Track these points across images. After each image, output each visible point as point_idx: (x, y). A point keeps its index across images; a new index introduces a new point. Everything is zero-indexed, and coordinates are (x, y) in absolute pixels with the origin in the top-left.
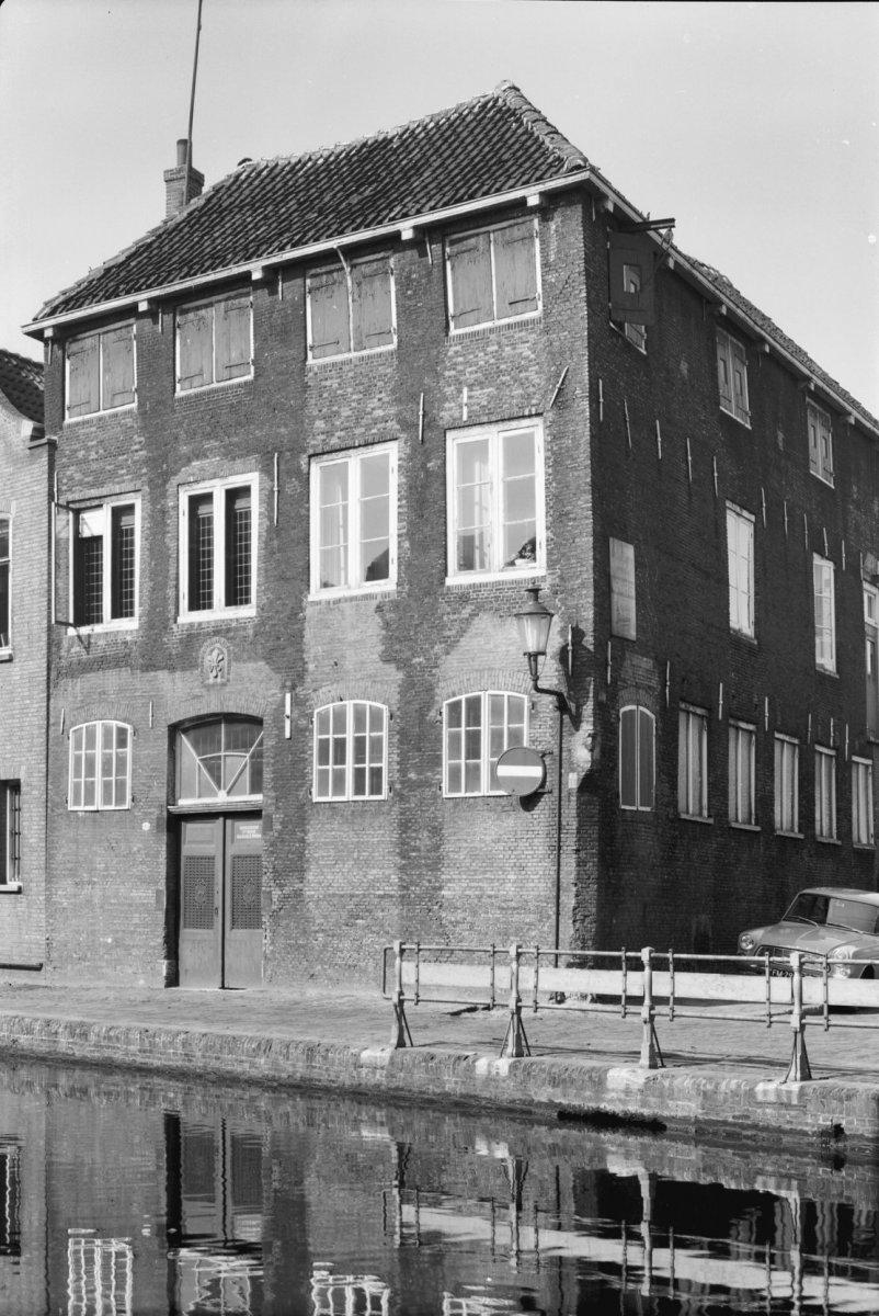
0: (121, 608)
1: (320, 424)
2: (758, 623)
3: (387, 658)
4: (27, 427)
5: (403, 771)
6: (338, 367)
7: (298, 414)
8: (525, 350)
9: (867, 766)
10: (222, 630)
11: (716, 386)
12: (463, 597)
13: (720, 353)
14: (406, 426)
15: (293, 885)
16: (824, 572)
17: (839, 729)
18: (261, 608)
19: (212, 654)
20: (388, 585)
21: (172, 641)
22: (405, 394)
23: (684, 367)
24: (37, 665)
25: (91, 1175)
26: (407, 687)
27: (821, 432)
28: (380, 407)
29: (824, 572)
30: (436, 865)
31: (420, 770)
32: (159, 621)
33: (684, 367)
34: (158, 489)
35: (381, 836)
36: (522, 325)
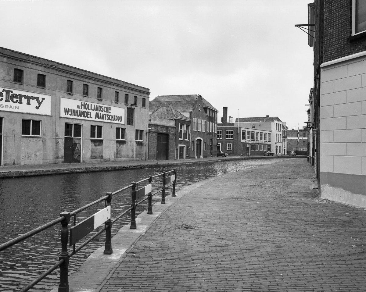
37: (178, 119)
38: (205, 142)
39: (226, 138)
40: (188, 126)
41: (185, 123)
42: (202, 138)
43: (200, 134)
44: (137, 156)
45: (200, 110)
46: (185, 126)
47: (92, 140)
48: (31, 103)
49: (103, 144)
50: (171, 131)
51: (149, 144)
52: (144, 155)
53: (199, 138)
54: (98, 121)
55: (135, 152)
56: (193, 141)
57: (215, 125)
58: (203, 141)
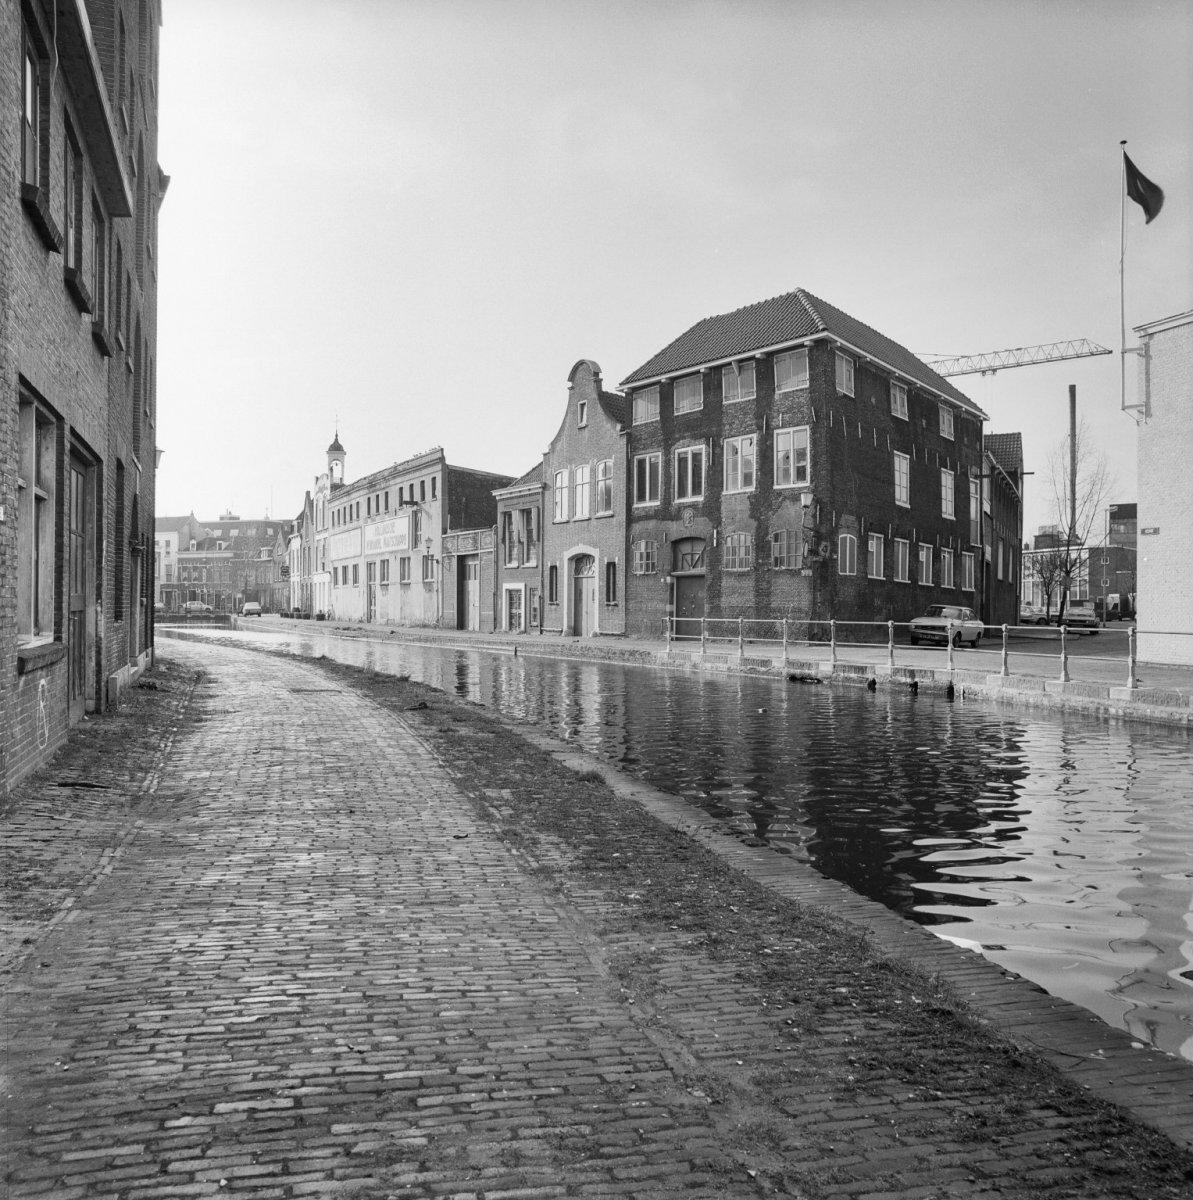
0: (653, 496)
1: (727, 427)
2: (912, 500)
3: (751, 517)
4: (619, 427)
5: (757, 559)
6: (734, 404)
7: (720, 425)
8: (802, 400)
9: (970, 557)
10: (693, 506)
11: (889, 404)
12: (780, 493)
13: (892, 391)
14: (760, 428)
15: (716, 602)
16: (947, 480)
17: (954, 540)
18: (706, 497)
19: (687, 514)
20: (752, 489)
21: (673, 509)
22: (759, 416)
23: (873, 400)
24: (622, 517)
25: (811, 839)
26: (758, 528)
27: (946, 416)
28: (750, 420)
29: (947, 480)
30: (768, 595)
31: (763, 559)
32: (667, 501)
33: (873, 400)
34: (667, 453)
35: (749, 584)
36: (801, 390)
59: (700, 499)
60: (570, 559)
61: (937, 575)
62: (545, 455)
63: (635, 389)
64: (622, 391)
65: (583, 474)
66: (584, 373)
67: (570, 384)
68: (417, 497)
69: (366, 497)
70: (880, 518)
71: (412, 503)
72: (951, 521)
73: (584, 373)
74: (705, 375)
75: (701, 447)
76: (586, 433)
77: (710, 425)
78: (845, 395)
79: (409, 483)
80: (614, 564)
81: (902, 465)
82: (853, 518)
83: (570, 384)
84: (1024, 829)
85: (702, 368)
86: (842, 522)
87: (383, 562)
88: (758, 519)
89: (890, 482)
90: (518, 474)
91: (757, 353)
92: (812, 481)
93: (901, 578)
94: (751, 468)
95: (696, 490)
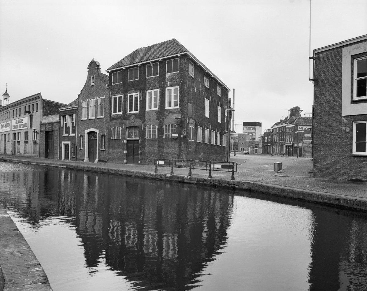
14: (160, 87)
16: (219, 108)
17: (221, 130)
19: (133, 118)
21: (127, 116)
22: (160, 82)
26: (159, 123)
29: (219, 108)
30: (163, 147)
37: (63, 110)
38: (103, 135)
39: (355, 152)
40: (71, 116)
41: (67, 114)
42: (97, 129)
43: (91, 123)
44: (33, 154)
45: (93, 84)
46: (68, 117)
47: (25, 141)
48: (286, 114)
49: (96, 132)
50: (56, 127)
51: (40, 143)
52: (37, 152)
53: (92, 129)
54: (20, 130)
55: (32, 150)
56: (81, 136)
57: (216, 136)
58: (99, 134)
59: (137, 112)
60: (87, 133)
61: (210, 140)
62: (79, 95)
63: (113, 71)
64: (108, 72)
65: (92, 102)
66: (94, 66)
67: (88, 70)
68: (31, 110)
69: (13, 110)
70: (201, 122)
71: (30, 112)
72: (220, 123)
73: (94, 66)
74: (140, 67)
75: (138, 94)
76: (94, 87)
77: (142, 86)
78: (191, 76)
79: (28, 105)
80: (104, 135)
81: (207, 103)
82: (193, 120)
83: (88, 70)
84: (308, 265)
85: (139, 64)
86: (190, 122)
87: (19, 133)
88: (159, 120)
89: (204, 109)
90: (67, 103)
91: (160, 59)
92: (180, 107)
93: (207, 142)
94: (177, 99)
95: (136, 110)
